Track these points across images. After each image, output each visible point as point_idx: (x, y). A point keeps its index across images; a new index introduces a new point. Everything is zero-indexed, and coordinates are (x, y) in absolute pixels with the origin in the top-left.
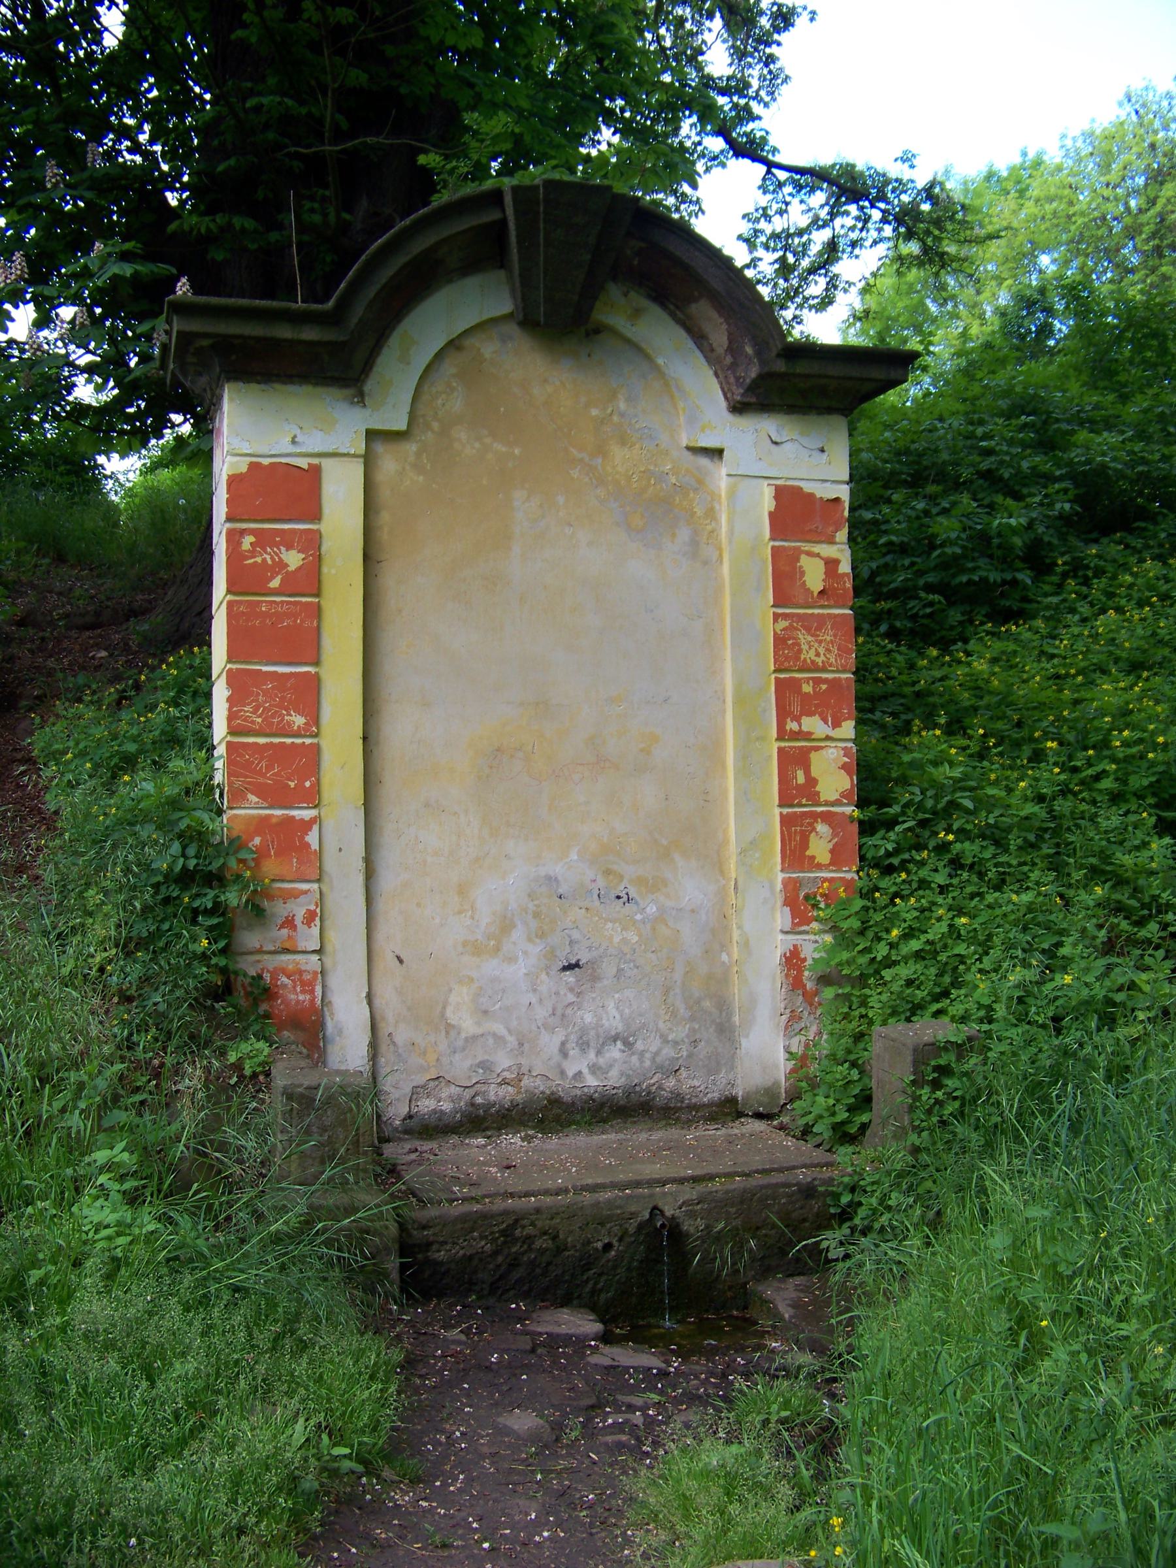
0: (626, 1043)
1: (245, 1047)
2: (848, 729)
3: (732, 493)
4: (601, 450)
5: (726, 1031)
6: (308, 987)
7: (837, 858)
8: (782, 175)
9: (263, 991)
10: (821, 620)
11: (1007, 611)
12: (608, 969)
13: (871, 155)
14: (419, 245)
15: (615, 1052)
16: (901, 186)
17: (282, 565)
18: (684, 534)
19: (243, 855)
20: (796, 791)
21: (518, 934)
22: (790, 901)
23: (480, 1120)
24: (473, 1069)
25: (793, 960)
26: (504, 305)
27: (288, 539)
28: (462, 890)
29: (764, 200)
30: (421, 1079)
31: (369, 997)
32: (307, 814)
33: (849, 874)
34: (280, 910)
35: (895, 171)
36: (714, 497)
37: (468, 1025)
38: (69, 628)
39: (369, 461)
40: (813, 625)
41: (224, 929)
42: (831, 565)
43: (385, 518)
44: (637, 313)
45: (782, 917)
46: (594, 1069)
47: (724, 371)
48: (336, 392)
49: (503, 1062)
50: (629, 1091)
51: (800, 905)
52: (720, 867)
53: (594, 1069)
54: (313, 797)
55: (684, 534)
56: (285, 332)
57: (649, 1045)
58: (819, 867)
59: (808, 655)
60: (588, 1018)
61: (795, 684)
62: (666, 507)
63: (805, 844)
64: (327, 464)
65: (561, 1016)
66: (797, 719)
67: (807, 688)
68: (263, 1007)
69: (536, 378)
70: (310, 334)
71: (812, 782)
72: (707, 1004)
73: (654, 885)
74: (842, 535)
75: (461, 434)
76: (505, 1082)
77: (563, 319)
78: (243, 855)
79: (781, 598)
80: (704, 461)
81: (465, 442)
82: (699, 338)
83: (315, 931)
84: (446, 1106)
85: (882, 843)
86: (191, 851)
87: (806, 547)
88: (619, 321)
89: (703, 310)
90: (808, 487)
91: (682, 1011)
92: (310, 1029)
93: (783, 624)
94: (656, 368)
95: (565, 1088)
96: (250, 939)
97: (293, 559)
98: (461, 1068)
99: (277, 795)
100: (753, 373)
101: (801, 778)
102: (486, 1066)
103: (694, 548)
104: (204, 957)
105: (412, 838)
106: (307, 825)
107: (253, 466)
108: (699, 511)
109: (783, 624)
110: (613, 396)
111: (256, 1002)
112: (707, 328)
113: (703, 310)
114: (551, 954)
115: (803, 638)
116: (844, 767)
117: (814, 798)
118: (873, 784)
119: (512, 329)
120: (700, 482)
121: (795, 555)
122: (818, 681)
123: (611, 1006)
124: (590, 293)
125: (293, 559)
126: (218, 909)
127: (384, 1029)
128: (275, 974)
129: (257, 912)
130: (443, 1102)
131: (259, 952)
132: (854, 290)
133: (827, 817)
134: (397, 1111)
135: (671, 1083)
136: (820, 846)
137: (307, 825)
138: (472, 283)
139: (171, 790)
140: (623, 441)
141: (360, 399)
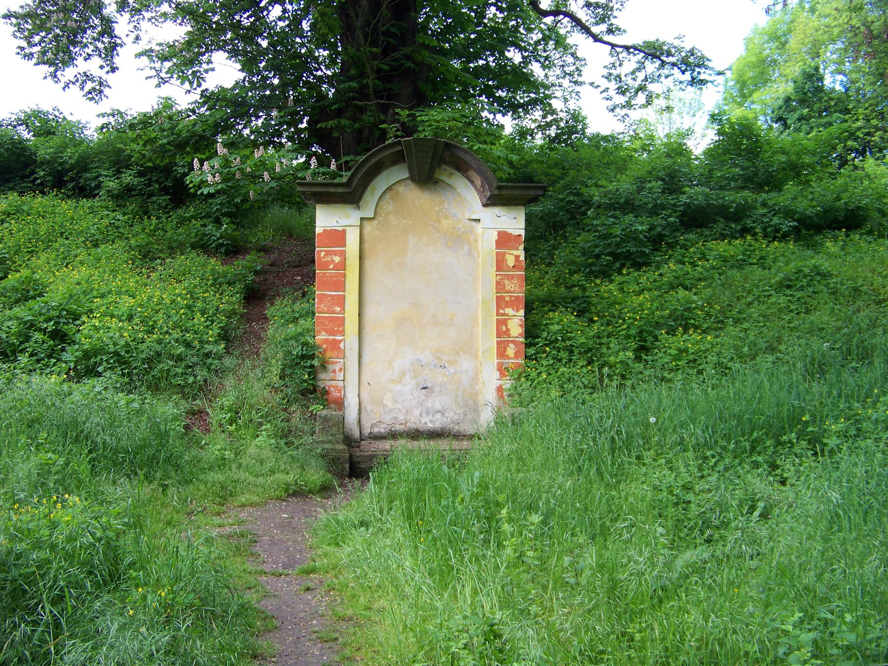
0: (443, 414)
1: (315, 406)
2: (522, 312)
3: (483, 234)
4: (439, 221)
5: (476, 411)
6: (339, 391)
7: (517, 355)
8: (619, 50)
9: (326, 392)
10: (513, 276)
11: (639, 263)
12: (437, 389)
13: (666, 36)
14: (375, 160)
15: (438, 416)
16: (679, 50)
17: (333, 261)
18: (466, 248)
19: (320, 350)
20: (502, 331)
21: (408, 377)
22: (500, 369)
23: (393, 435)
24: (391, 419)
25: (500, 389)
26: (407, 175)
27: (335, 253)
28: (390, 362)
29: (613, 60)
30: (374, 422)
31: (359, 395)
32: (339, 338)
33: (521, 361)
34: (331, 367)
35: (676, 43)
36: (477, 235)
37: (390, 405)
38: (289, 267)
39: (361, 227)
40: (510, 278)
41: (313, 373)
42: (517, 257)
43: (366, 246)
44: (451, 175)
45: (497, 374)
46: (431, 421)
47: (480, 193)
48: (350, 206)
49: (401, 417)
50: (442, 429)
51: (502, 370)
52: (476, 357)
53: (431, 421)
54: (342, 333)
55: (466, 248)
56: (332, 190)
57: (450, 414)
58: (510, 358)
59: (508, 288)
60: (430, 405)
61: (503, 298)
62: (459, 240)
63: (505, 350)
64: (347, 228)
65: (421, 404)
66: (504, 309)
67: (507, 299)
68: (326, 397)
69: (415, 197)
70: (340, 190)
71: (508, 330)
72: (470, 402)
73: (454, 363)
74: (522, 247)
75: (391, 217)
76: (401, 424)
77: (426, 177)
78: (320, 350)
79: (499, 268)
80: (474, 223)
81: (393, 220)
82: (472, 182)
83: (342, 374)
84: (382, 431)
85: (531, 351)
86: (304, 349)
87: (508, 251)
88: (444, 178)
89: (472, 173)
90: (509, 231)
91: (461, 404)
92: (340, 404)
93: (499, 277)
94: (458, 193)
95: (421, 427)
96: (322, 376)
97: (337, 259)
98: (387, 419)
99: (331, 332)
100: (489, 194)
101: (504, 328)
102: (396, 418)
103: (470, 253)
104: (305, 381)
105: (374, 346)
106: (340, 341)
107: (324, 230)
108: (472, 240)
109: (499, 277)
110: (443, 202)
111: (323, 395)
112: (474, 179)
113: (472, 173)
114: (418, 384)
115: (506, 282)
116: (520, 325)
117: (509, 335)
118: (531, 332)
119: (410, 182)
120: (472, 230)
121: (504, 254)
122: (511, 296)
123: (437, 401)
124: (432, 171)
125: (337, 259)
126: (312, 366)
127: (363, 405)
128: (329, 387)
129: (324, 366)
130: (381, 429)
131: (325, 380)
132: (661, 98)
133: (513, 342)
134: (366, 431)
135: (457, 427)
136: (511, 351)
137: (340, 341)
138: (395, 168)
139: (299, 330)
140: (446, 217)
141: (358, 208)
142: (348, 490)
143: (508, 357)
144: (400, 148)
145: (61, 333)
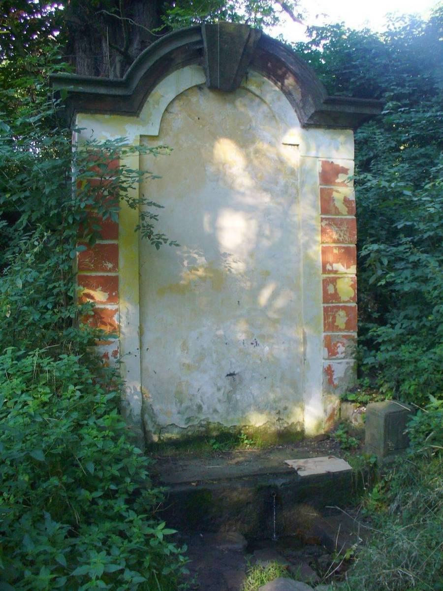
7: (348, 327)
44: (260, 85)
47: (300, 108)
56: (102, 91)
58: (340, 330)
136: (341, 319)
142: (12, 360)
143: (337, 329)
144: (196, 38)
145: (359, 188)
